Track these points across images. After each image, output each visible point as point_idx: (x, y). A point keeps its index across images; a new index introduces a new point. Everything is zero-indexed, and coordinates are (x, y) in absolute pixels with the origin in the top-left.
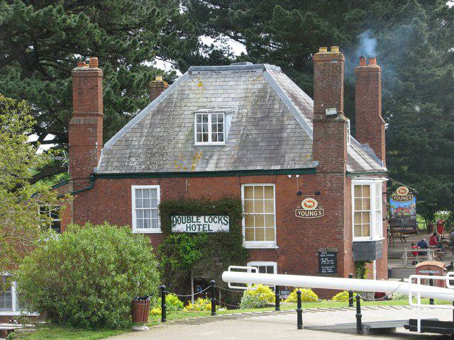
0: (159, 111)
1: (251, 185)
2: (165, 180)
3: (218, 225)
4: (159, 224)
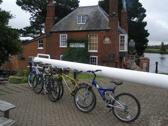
0: (70, 17)
1: (91, 34)
2: (68, 33)
3: (82, 46)
4: (67, 45)
